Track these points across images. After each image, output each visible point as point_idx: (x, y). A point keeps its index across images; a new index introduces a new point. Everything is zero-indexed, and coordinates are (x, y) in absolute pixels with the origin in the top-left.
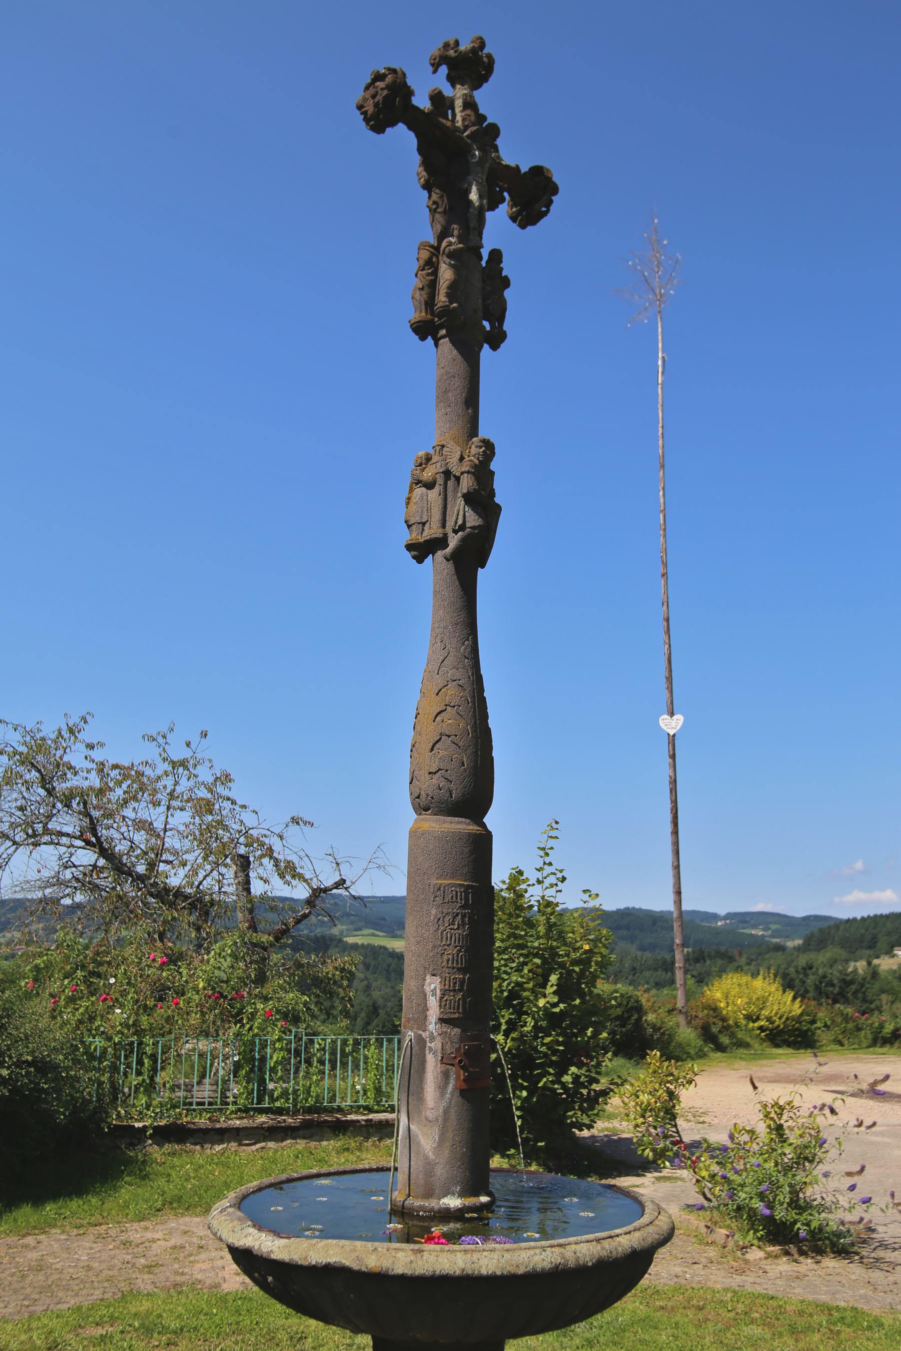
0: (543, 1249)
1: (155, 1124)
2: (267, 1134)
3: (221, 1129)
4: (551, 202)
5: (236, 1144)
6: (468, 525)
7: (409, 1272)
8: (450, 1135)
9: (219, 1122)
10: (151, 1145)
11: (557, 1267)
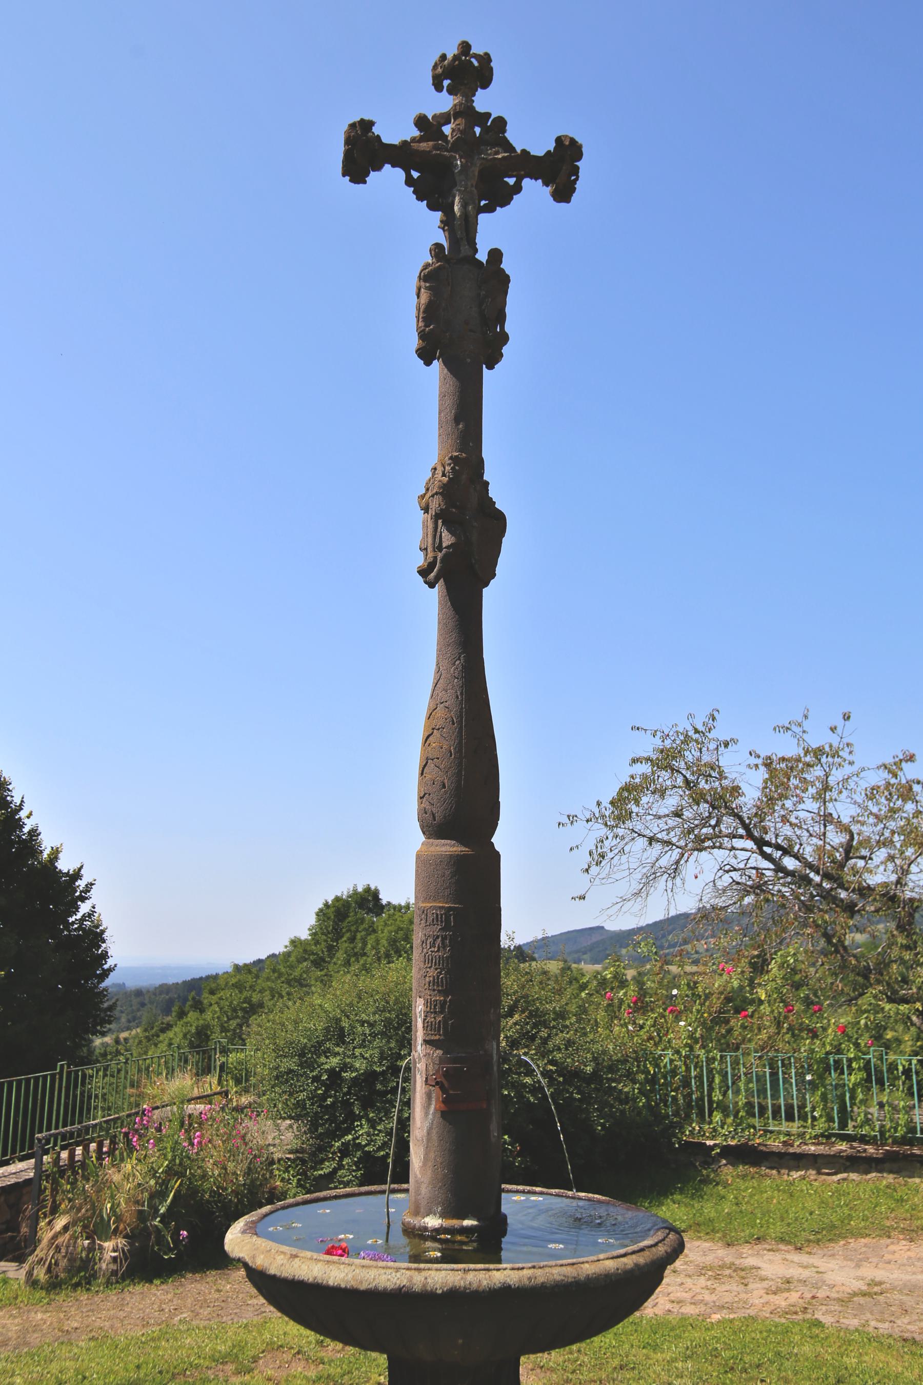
0: (398, 1270)
1: (725, 1143)
2: (848, 1164)
3: (795, 1154)
4: (578, 168)
5: (814, 1172)
6: (444, 545)
7: (278, 1274)
8: (432, 1155)
9: (792, 1146)
10: (725, 1165)
11: (400, 1289)
